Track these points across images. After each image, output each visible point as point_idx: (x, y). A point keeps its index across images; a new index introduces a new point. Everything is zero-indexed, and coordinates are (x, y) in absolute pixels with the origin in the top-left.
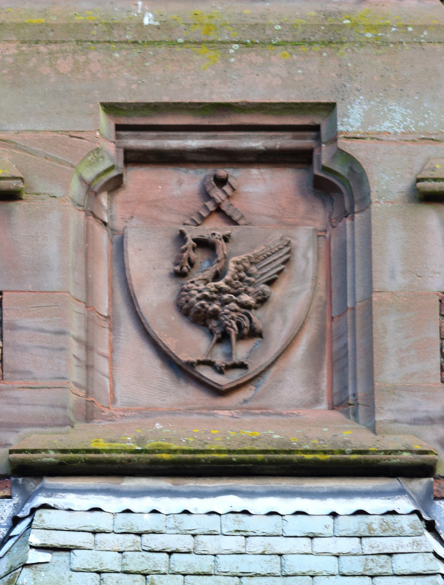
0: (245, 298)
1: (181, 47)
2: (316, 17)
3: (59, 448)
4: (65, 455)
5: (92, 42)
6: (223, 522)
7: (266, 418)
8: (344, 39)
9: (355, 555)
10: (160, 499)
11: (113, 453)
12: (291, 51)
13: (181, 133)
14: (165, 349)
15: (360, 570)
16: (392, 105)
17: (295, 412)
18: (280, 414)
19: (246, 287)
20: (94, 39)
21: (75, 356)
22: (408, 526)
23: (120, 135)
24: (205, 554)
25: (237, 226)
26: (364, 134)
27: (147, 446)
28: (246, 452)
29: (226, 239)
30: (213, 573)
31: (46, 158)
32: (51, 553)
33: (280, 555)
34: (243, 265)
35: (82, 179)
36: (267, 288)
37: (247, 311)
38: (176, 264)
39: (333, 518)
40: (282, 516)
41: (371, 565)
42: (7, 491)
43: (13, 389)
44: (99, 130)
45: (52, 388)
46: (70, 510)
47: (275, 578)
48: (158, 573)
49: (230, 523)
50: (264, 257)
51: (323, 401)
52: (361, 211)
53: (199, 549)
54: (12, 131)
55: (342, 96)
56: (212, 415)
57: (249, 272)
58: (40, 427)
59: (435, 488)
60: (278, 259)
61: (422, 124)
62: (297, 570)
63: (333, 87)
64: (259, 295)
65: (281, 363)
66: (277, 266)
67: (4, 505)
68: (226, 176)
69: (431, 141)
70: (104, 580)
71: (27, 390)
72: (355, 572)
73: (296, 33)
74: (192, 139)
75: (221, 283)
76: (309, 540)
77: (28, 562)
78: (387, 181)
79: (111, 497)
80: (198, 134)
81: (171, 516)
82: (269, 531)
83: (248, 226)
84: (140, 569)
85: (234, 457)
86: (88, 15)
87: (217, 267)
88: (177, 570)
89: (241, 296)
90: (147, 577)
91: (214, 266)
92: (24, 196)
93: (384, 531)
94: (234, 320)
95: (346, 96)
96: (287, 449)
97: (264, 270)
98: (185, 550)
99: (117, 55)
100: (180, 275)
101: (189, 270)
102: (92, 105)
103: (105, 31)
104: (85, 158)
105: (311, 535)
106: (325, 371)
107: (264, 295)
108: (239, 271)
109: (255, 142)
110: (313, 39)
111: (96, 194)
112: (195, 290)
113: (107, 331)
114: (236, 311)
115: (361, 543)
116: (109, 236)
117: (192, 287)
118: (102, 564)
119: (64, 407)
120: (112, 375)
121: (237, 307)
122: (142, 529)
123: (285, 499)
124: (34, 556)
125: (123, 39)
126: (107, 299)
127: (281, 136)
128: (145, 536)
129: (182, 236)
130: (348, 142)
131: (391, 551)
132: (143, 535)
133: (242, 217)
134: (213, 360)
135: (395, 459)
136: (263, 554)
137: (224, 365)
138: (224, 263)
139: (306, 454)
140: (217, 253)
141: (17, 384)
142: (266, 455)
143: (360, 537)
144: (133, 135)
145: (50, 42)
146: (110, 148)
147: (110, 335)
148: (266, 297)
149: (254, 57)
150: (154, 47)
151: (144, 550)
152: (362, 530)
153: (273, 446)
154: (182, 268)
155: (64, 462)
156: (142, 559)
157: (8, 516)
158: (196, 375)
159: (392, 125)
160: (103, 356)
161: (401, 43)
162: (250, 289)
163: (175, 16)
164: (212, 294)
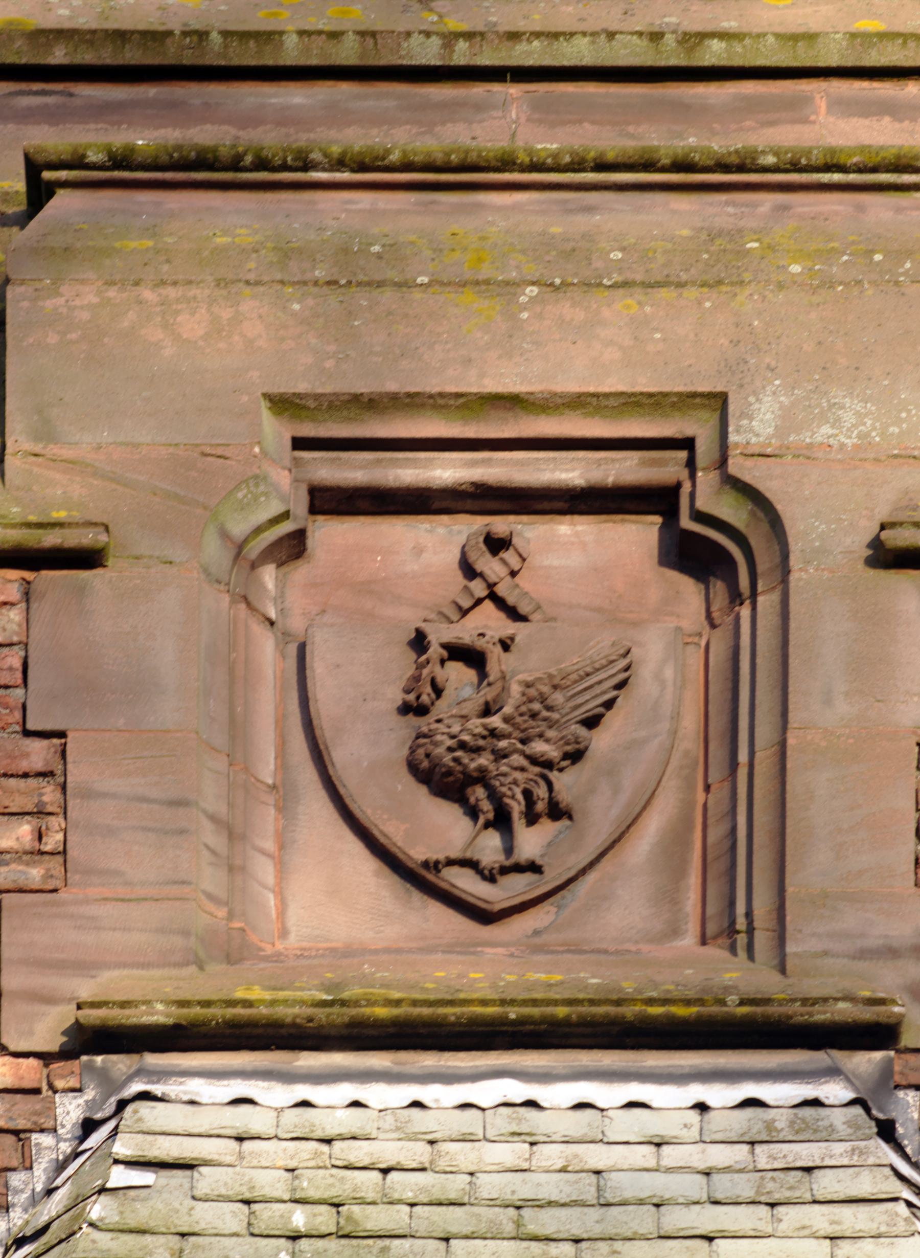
0: (539, 747)
1: (424, 292)
2: (691, 238)
3: (174, 998)
4: (185, 1011)
5: (248, 283)
6: (487, 1120)
7: (577, 957)
8: (747, 276)
9: (741, 1171)
10: (368, 1086)
11: (279, 1006)
12: (642, 298)
14: (382, 840)
15: (748, 1193)
16: (837, 394)
17: (633, 948)
18: (605, 952)
20: (252, 277)
21: (207, 846)
22: (844, 1123)
23: (302, 458)
24: (452, 1172)
25: (527, 623)
26: (781, 447)
27: (346, 995)
28: (535, 1002)
29: (506, 645)
30: (466, 1200)
31: (155, 494)
32: (156, 1172)
33: (598, 1173)
34: (537, 690)
35: (224, 535)
36: (582, 731)
37: (546, 771)
38: (407, 691)
39: (701, 1114)
40: (602, 1110)
41: (770, 1186)
42: (72, 1079)
43: (87, 901)
44: (259, 443)
45: (163, 899)
46: (192, 1102)
47: (586, 1209)
48: (362, 1202)
49: (502, 1121)
50: (580, 676)
51: (687, 931)
53: (440, 1163)
54: (87, 443)
55: (740, 379)
56: (474, 953)
57: (549, 702)
58: (138, 968)
59: (897, 1068)
60: (606, 679)
61: (894, 430)
62: (628, 1194)
63: (723, 364)
64: (567, 744)
65: (605, 865)
66: (604, 693)
67: (67, 1104)
68: (508, 533)
69: (912, 461)
70: (257, 1213)
71: (113, 903)
72: (738, 1197)
73: (652, 266)
75: (495, 721)
76: (652, 1148)
77: (108, 1185)
78: (826, 529)
79: (273, 1083)
81: (389, 1112)
82: (575, 1133)
83: (547, 624)
84: (326, 1195)
85: (513, 1014)
86: (239, 235)
87: (488, 694)
88: (396, 1196)
89: (533, 744)
90: (340, 1209)
91: (482, 693)
92: (110, 563)
93: (797, 1132)
94: (518, 786)
95: (748, 380)
96: (615, 997)
97: (580, 700)
98: (414, 1165)
99: (296, 307)
100: (413, 709)
102: (245, 398)
103: (272, 262)
104: (231, 492)
105: (657, 1140)
106: (694, 879)
107: (578, 743)
108: (531, 701)
110: (684, 277)
111: (254, 566)
112: (443, 734)
113: (272, 811)
114: (522, 769)
115: (753, 1152)
116: (277, 645)
117: (437, 729)
118: (254, 1187)
119: (186, 933)
120: (281, 888)
121: (524, 762)
122: (330, 1132)
123: (608, 1085)
124: (119, 1176)
125: (308, 276)
126: (273, 755)
127: (618, 460)
128: (337, 1145)
129: (419, 642)
130: (749, 463)
131: (810, 1164)
132: (334, 1143)
133: (538, 607)
135: (821, 1015)
136: (563, 1170)
137: (497, 865)
138: (500, 689)
139: (651, 1006)
140: (488, 669)
141: (94, 892)
142: (573, 1009)
143: (752, 1143)
144: (326, 460)
145: (163, 283)
146: (283, 478)
147: (276, 819)
148: (581, 746)
149: (568, 309)
150: (370, 292)
151: (334, 1166)
152: (754, 1131)
153: (589, 993)
154: (418, 697)
155: (184, 1023)
156: (331, 1181)
157: (74, 1121)
159: (835, 431)
160: (263, 852)
161: (859, 282)
162: (551, 734)
163: (413, 238)
164: (476, 740)
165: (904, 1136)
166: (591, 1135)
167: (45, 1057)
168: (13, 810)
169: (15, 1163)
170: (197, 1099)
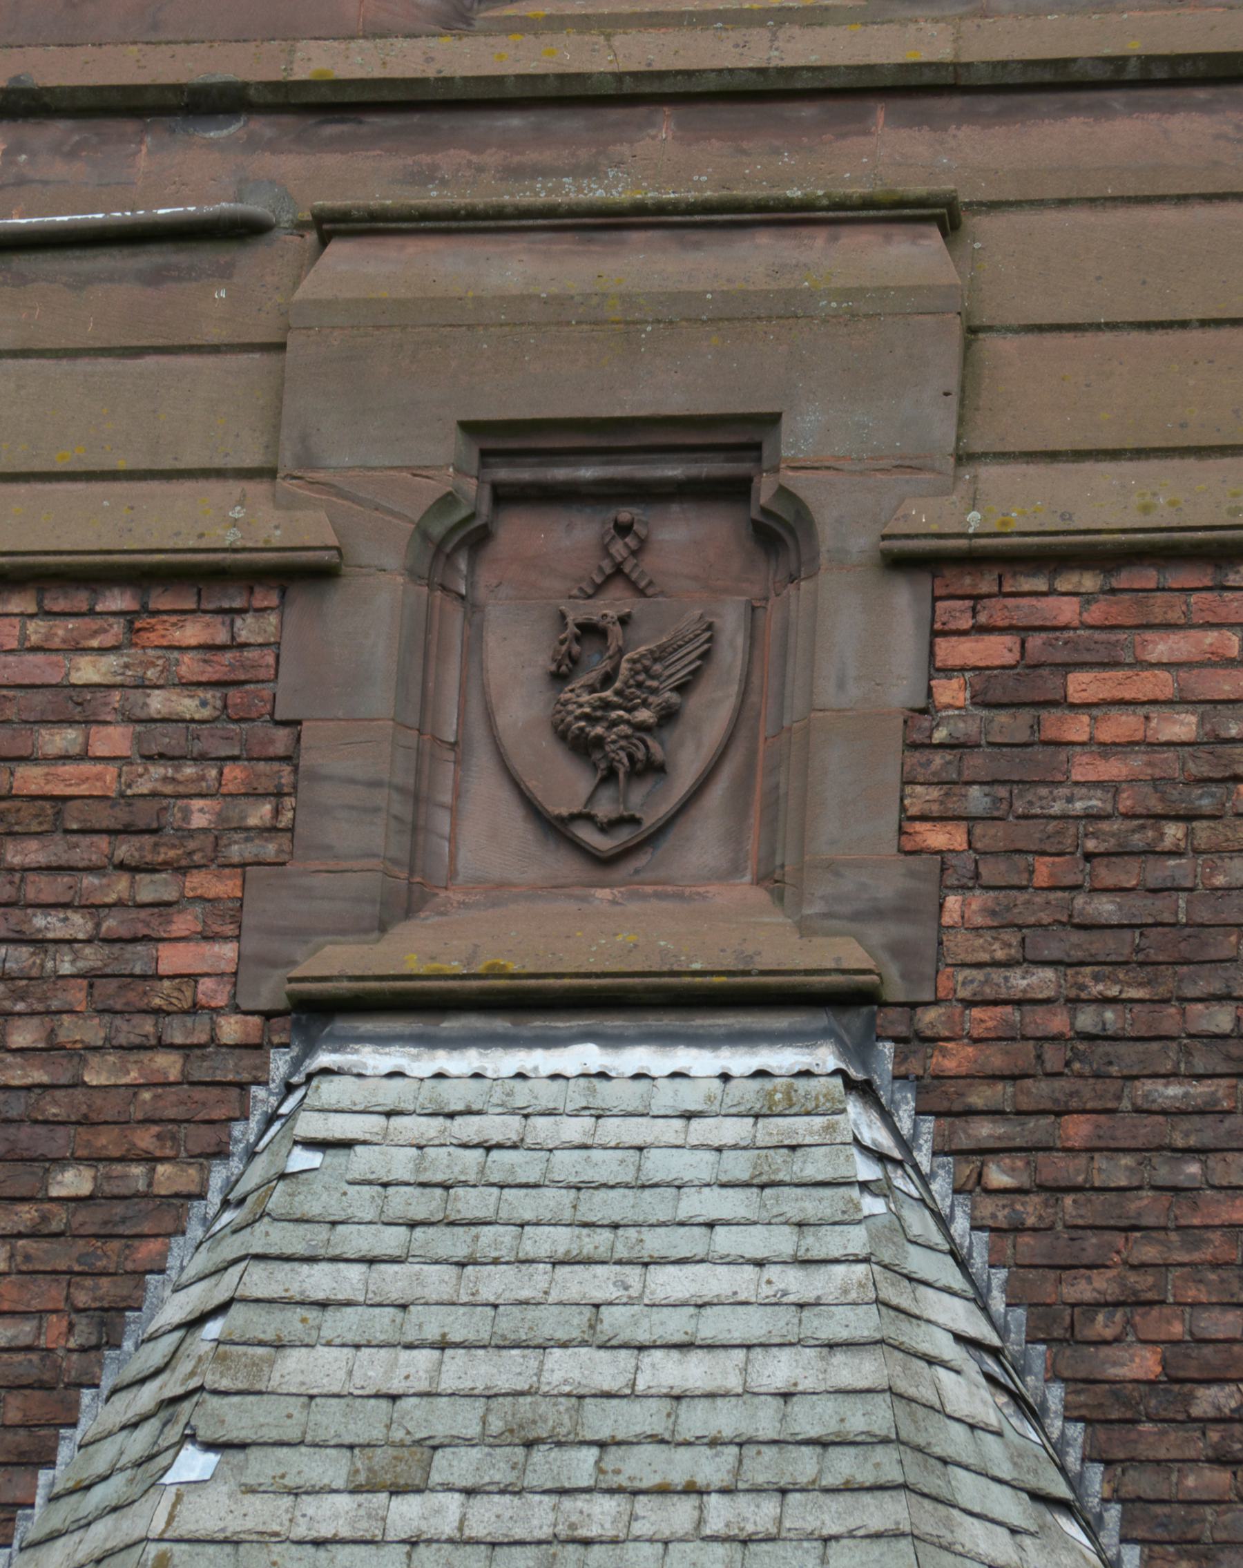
0: (644, 715)
13: (572, 458)
19: (644, 696)
29: (624, 621)
48: (465, 1184)
52: (808, 577)
66: (690, 663)
74: (588, 465)
75: (608, 694)
80: (595, 458)
88: (492, 1180)
100: (559, 678)
101: (570, 670)
108: (637, 673)
109: (673, 469)
113: (452, 766)
134: (593, 812)
158: (569, 835)
160: (442, 806)
165: (879, 1087)
166: (641, 1109)
167: (268, 1015)
168: (261, 791)
169: (237, 1114)
170: (364, 1072)
